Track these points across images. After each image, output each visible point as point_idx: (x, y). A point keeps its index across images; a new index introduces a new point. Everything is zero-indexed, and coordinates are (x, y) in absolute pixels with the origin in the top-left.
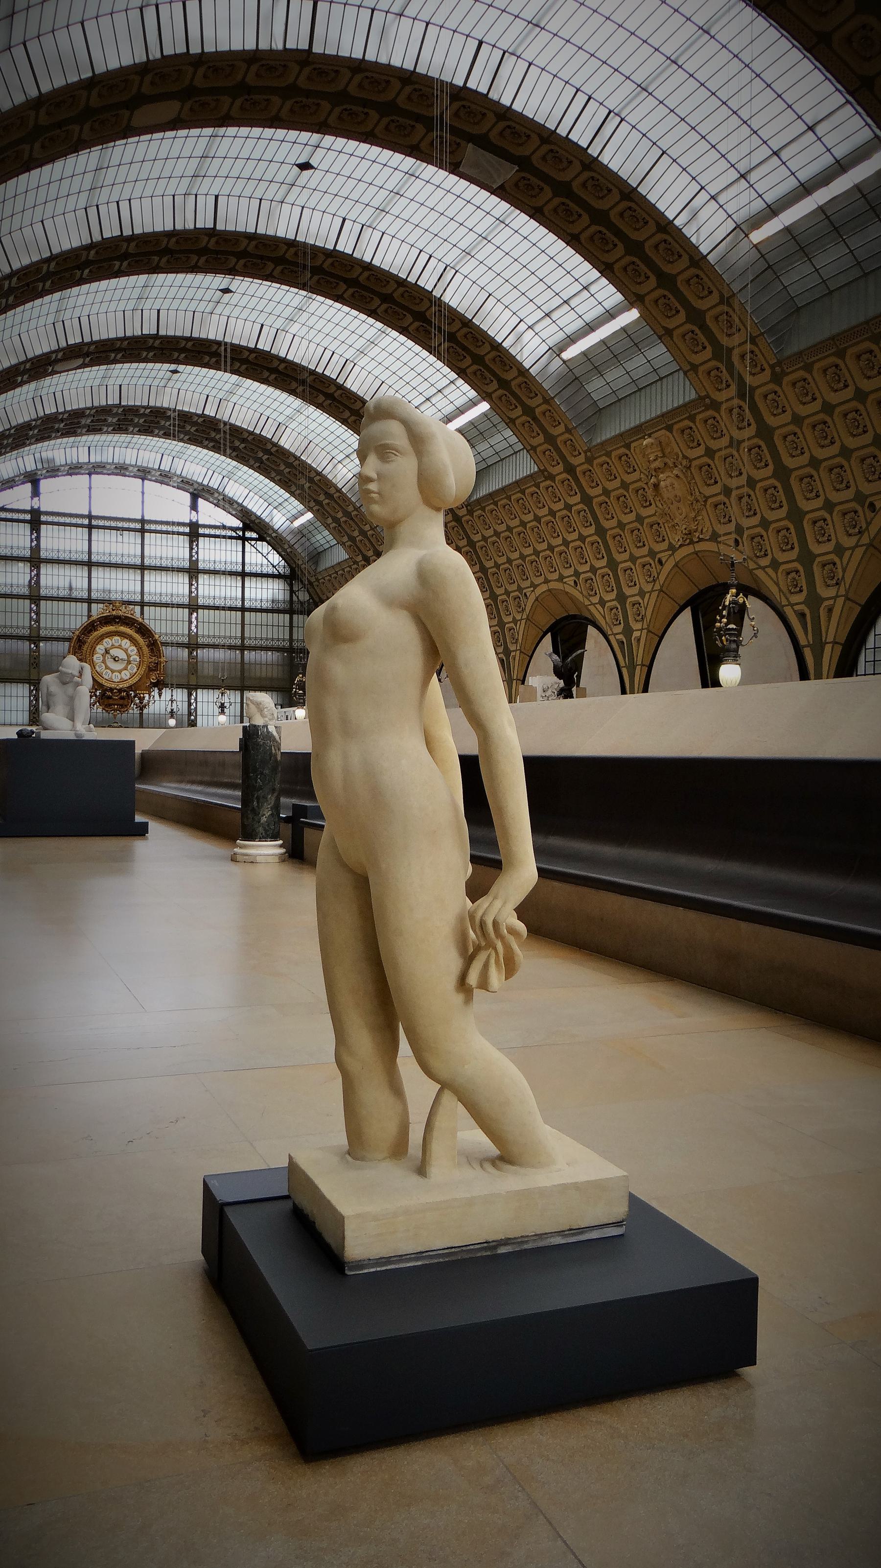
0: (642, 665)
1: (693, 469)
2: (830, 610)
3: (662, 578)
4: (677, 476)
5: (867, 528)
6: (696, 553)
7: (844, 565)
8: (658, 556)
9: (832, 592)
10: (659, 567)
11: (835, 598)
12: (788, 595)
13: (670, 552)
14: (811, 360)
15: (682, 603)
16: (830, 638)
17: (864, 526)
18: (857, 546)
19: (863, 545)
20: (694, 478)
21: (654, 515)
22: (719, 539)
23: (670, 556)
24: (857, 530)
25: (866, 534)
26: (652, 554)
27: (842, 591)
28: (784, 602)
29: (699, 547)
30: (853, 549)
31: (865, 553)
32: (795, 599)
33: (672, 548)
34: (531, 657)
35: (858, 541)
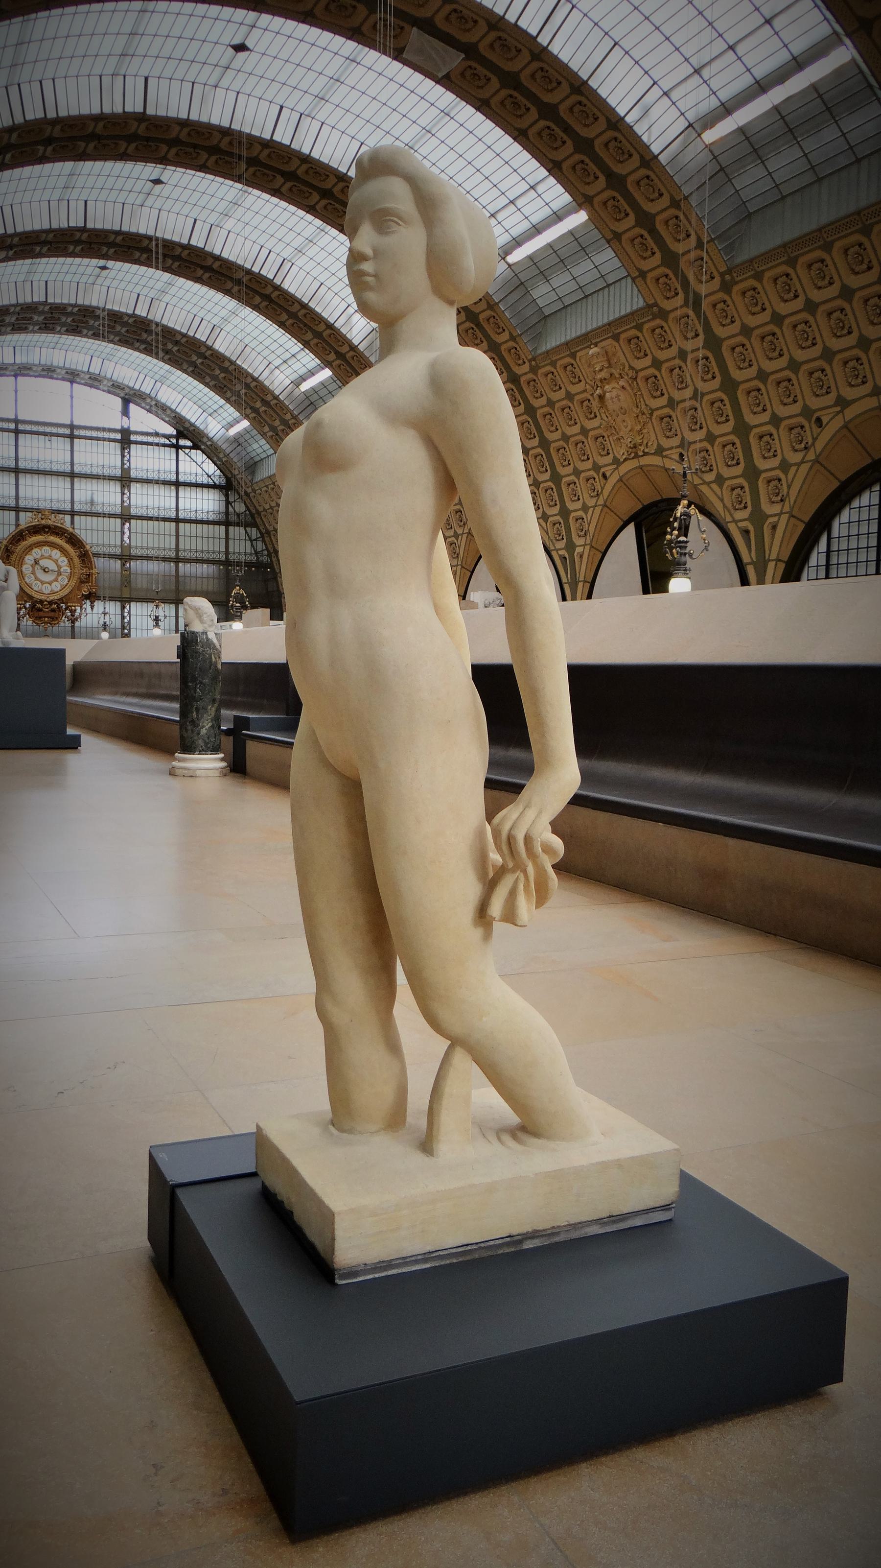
0: (585, 582)
1: (639, 380)
2: (774, 527)
3: (606, 493)
4: (623, 387)
5: (813, 444)
6: (641, 467)
7: (790, 481)
8: (602, 470)
9: (776, 509)
10: (603, 481)
11: (779, 515)
12: (733, 511)
13: (839, 409)
14: (761, 269)
15: (625, 518)
16: (774, 556)
17: (810, 441)
18: (802, 462)
19: (807, 462)
20: (640, 390)
21: (599, 427)
22: (664, 453)
23: (615, 470)
24: (803, 446)
25: (812, 449)
26: (596, 467)
27: (787, 508)
28: (728, 519)
29: (645, 461)
30: (799, 464)
31: (811, 468)
32: (739, 515)
33: (617, 462)
34: (604, 554)
35: (804, 458)
